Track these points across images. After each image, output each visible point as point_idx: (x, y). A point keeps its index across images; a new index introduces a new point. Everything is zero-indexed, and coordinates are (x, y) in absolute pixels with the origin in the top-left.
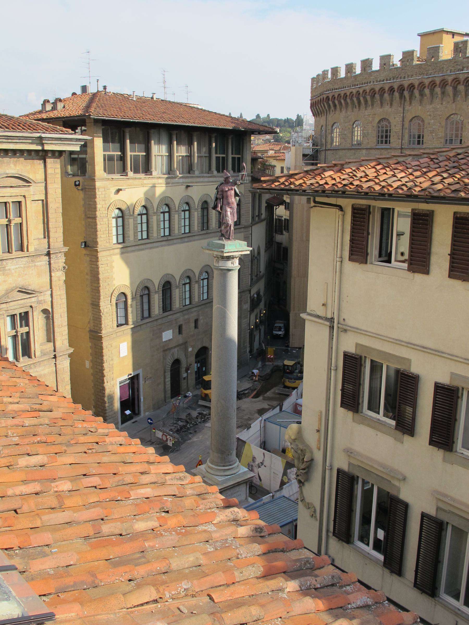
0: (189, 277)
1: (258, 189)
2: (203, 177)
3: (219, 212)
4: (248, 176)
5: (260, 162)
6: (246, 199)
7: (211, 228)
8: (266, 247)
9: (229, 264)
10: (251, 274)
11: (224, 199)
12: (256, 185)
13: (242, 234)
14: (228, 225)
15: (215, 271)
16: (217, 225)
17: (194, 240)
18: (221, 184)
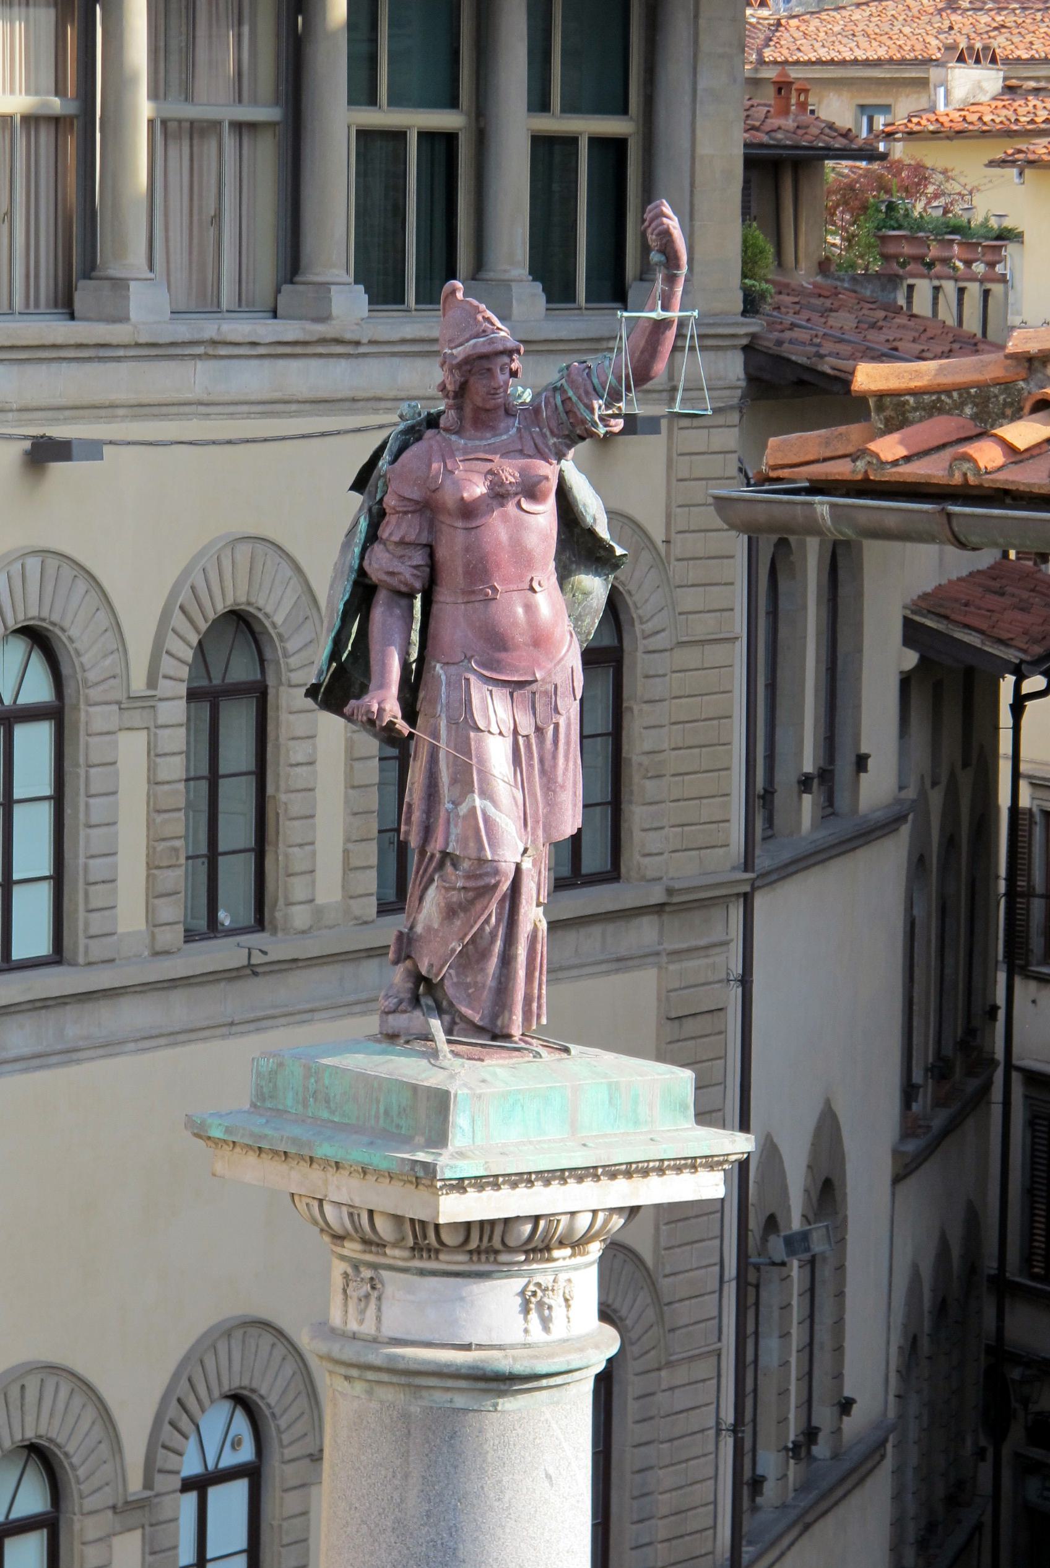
0: (41, 1456)
1: (818, 488)
2: (215, 349)
3: (389, 736)
4: (710, 341)
5: (849, 193)
6: (690, 600)
7: (300, 917)
8: (909, 1128)
9: (493, 1316)
10: (743, 1429)
11: (444, 596)
12: (795, 448)
13: (644, 983)
14: (484, 888)
15: (330, 1384)
16: (369, 881)
17: (110, 1046)
18: (412, 434)
